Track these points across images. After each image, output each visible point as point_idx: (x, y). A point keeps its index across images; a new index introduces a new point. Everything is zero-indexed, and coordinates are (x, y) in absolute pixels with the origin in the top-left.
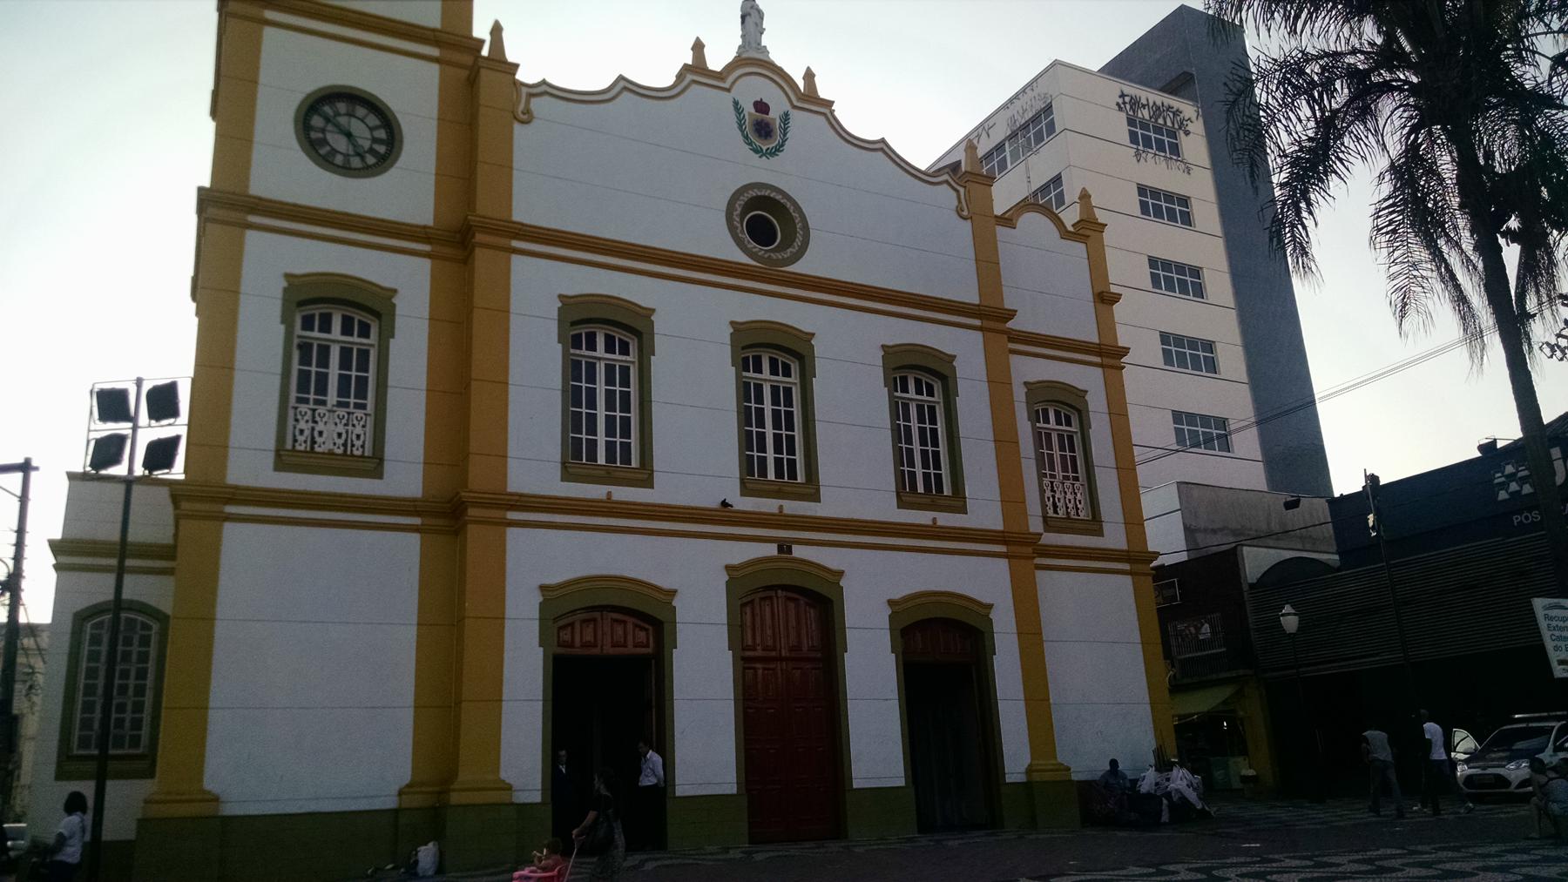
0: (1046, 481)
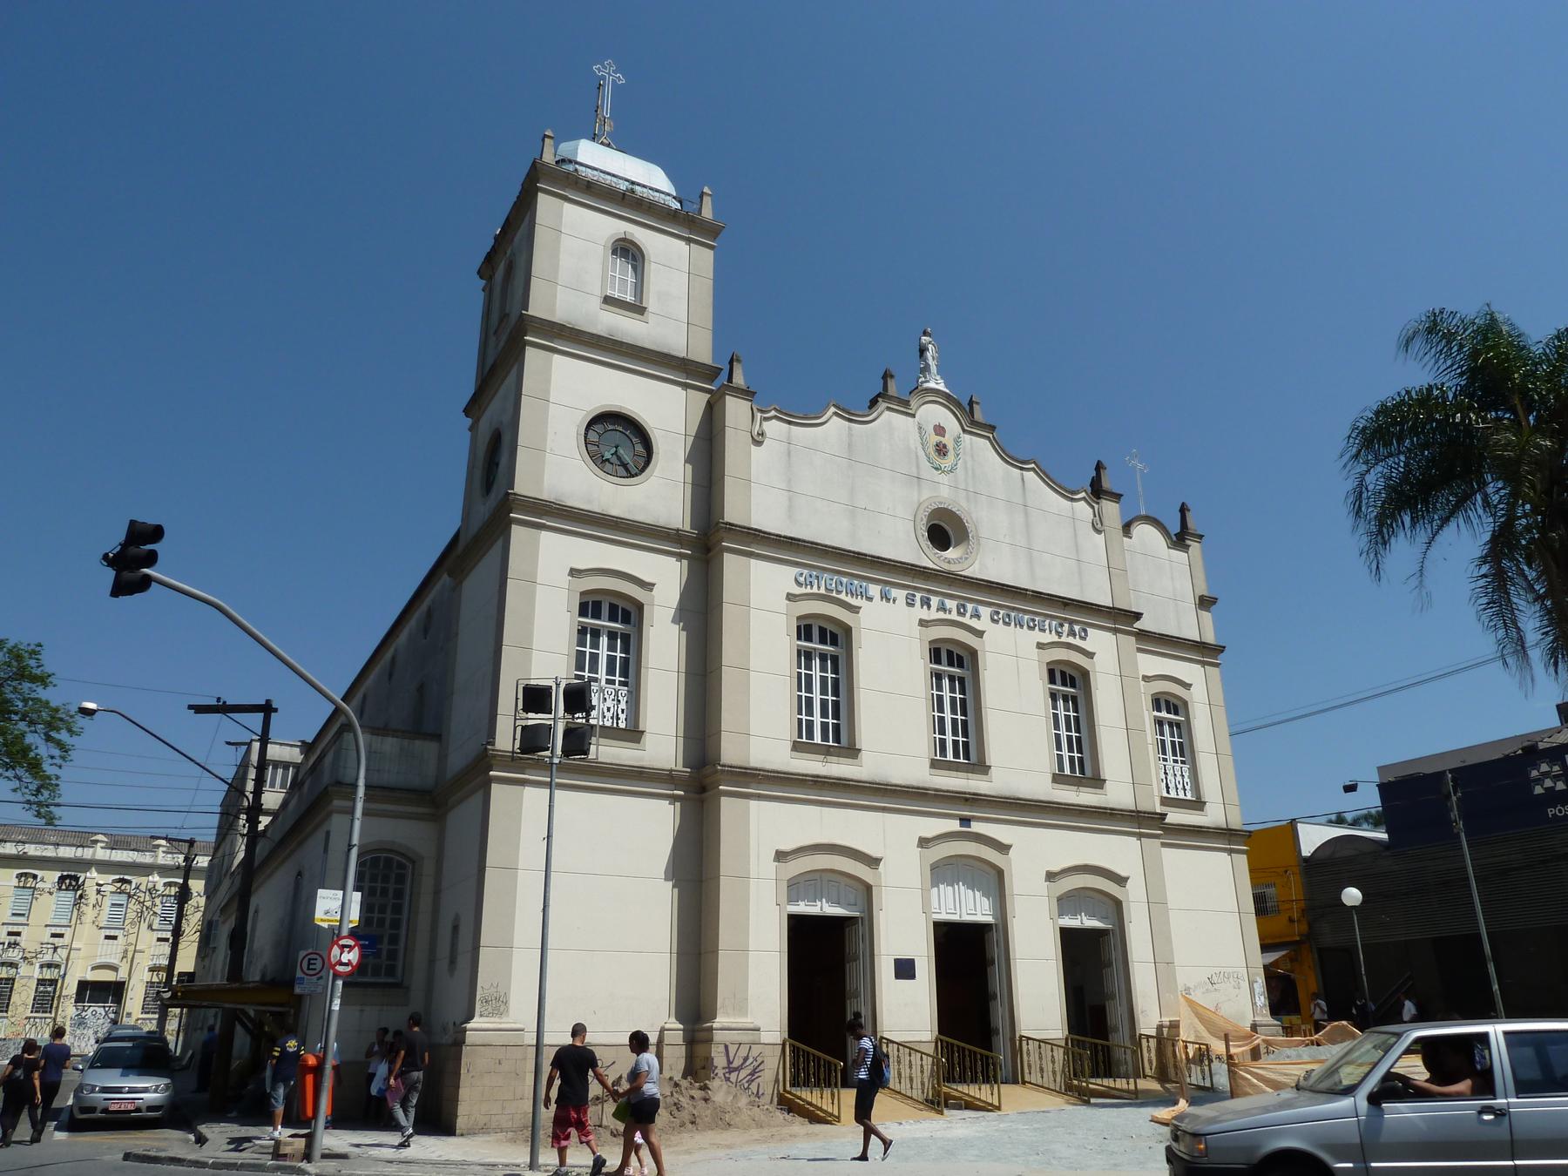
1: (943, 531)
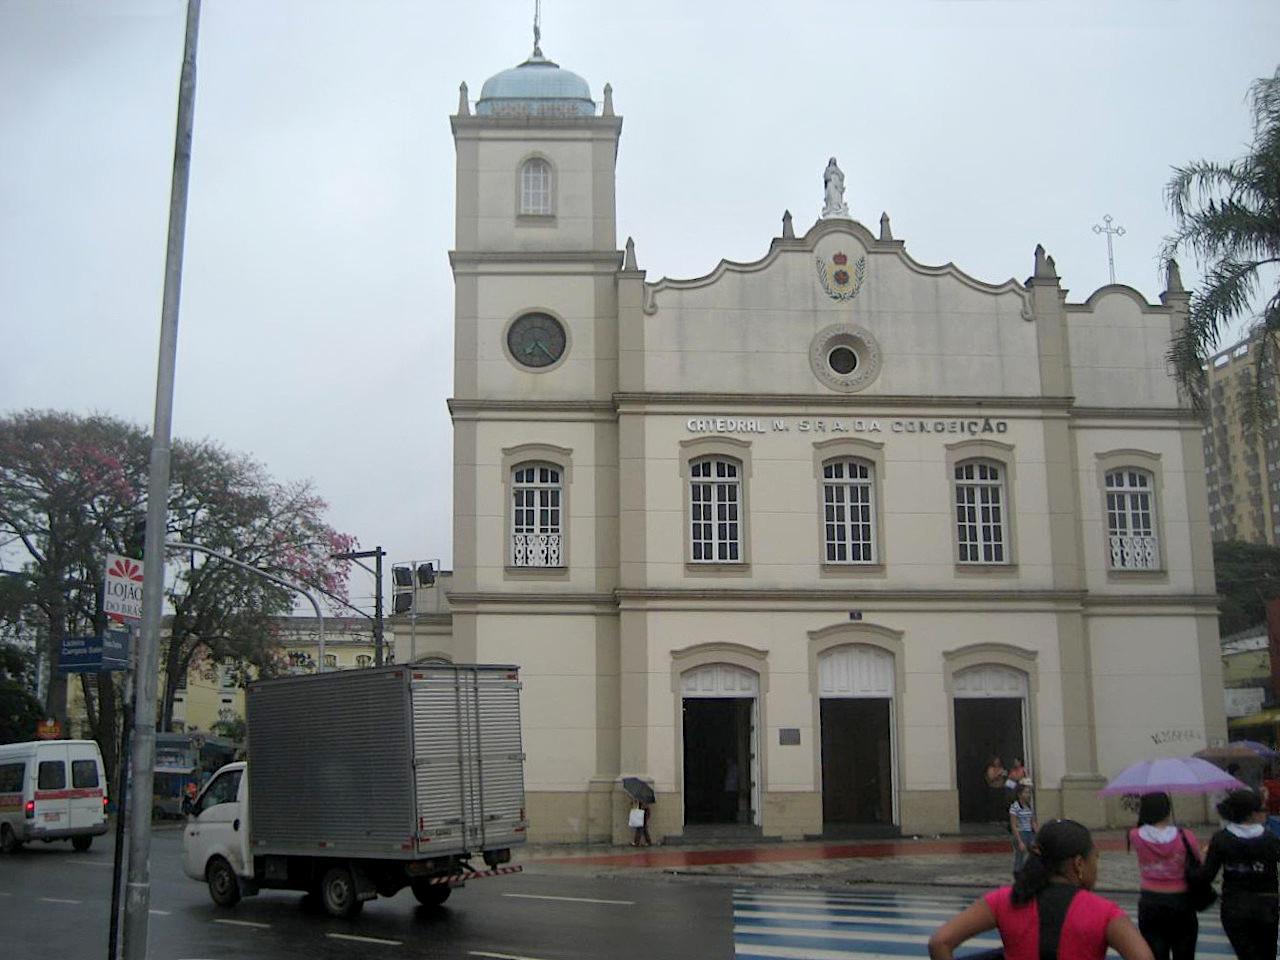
0: (1116, 539)
1: (843, 358)
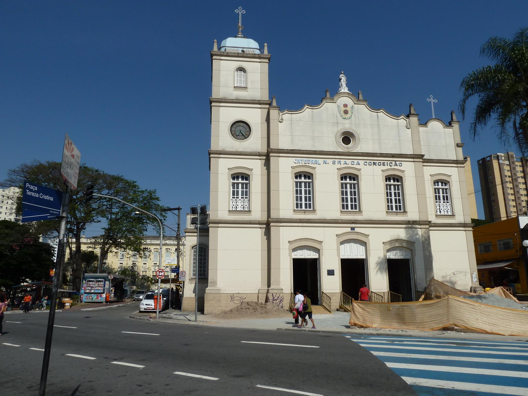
1: (347, 138)
